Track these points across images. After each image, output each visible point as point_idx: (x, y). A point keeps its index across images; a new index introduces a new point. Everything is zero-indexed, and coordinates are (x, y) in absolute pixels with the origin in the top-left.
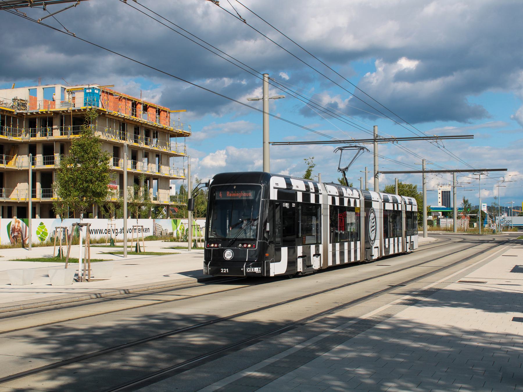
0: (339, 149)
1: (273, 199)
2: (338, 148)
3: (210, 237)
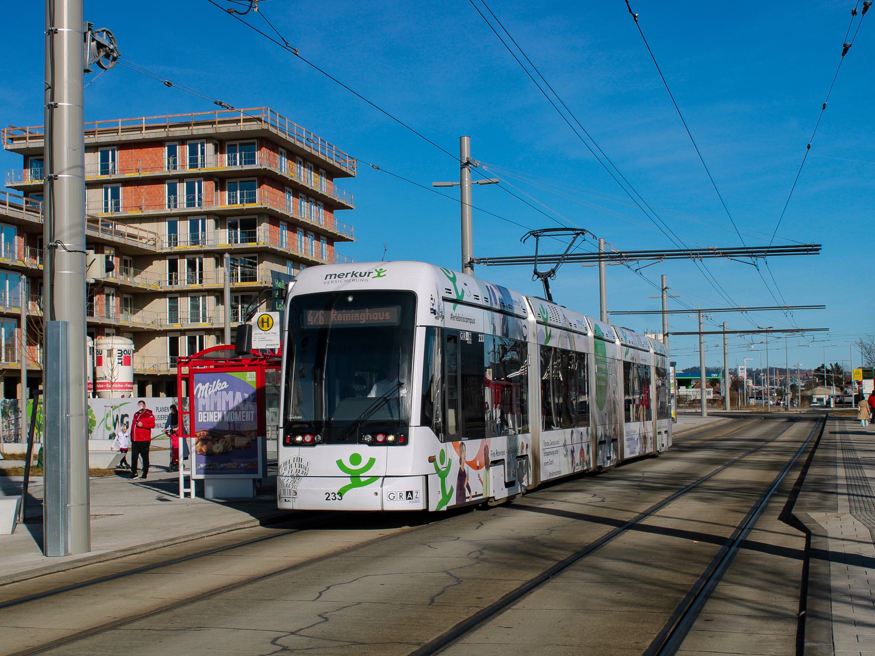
0: (531, 234)
1: (195, 378)
2: (530, 232)
3: (291, 418)
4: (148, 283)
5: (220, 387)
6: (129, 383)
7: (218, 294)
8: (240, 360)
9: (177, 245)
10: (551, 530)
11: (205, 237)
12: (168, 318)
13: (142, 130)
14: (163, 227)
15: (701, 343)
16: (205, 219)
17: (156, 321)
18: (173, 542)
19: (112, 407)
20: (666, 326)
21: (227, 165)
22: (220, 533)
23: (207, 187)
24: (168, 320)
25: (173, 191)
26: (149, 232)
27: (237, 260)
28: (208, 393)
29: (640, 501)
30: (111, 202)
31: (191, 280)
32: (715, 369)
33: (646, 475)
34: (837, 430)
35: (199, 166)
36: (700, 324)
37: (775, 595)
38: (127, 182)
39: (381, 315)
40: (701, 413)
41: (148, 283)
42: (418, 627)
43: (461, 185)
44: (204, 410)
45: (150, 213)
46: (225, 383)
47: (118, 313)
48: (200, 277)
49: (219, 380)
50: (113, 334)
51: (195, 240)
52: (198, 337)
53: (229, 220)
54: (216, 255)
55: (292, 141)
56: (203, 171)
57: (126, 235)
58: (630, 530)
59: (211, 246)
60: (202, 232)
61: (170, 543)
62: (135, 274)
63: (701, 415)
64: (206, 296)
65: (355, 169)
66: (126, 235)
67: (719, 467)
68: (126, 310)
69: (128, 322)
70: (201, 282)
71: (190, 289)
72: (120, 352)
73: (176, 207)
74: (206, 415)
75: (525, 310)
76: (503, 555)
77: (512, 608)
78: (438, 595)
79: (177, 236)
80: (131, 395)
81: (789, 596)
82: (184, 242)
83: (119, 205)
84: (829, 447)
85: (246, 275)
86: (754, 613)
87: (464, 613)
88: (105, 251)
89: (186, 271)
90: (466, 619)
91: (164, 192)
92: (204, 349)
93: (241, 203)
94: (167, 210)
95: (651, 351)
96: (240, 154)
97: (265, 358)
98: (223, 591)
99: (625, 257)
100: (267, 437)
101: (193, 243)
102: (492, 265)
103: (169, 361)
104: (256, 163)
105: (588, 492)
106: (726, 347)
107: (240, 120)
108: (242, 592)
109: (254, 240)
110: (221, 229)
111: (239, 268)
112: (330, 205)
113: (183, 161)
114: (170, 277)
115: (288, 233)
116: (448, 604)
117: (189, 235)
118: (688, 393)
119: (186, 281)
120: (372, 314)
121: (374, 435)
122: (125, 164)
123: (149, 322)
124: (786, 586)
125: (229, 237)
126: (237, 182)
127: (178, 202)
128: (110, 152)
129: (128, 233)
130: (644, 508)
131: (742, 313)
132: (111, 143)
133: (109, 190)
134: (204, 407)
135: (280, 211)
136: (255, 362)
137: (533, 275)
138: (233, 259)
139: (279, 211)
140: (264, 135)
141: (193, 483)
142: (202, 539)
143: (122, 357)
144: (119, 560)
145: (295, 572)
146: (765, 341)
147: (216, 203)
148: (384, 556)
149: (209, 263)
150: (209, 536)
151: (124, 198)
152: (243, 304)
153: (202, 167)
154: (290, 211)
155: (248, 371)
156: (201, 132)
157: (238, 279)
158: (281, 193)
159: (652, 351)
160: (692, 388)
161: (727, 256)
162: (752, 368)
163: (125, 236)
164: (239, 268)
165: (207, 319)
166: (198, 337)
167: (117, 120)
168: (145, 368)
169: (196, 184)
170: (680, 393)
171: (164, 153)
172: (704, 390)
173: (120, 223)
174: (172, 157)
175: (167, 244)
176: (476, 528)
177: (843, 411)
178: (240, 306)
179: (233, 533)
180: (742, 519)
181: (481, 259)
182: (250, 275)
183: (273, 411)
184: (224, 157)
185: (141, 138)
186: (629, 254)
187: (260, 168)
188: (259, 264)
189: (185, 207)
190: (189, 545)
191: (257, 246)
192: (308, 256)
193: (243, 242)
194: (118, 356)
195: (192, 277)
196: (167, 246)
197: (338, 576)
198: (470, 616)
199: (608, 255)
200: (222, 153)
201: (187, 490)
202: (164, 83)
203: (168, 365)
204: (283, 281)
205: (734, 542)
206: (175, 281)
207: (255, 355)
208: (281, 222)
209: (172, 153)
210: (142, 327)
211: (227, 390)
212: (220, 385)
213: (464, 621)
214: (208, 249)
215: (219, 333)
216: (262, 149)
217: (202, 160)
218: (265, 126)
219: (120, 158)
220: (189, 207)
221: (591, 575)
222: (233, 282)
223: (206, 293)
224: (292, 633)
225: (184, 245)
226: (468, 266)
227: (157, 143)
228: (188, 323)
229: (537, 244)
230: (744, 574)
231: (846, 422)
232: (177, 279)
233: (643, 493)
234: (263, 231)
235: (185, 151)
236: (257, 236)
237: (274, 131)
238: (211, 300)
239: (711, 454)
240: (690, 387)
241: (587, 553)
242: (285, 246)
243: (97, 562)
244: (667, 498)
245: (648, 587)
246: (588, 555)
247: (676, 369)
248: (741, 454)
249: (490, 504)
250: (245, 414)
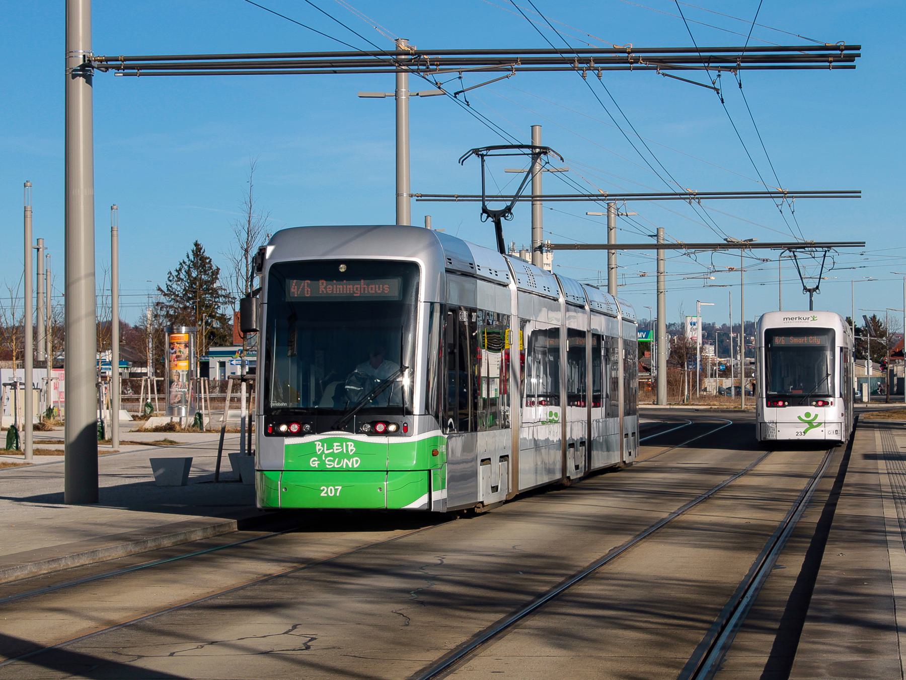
3: (272, 405)
15: (610, 269)
20: (538, 231)
32: (645, 323)
34: (879, 450)
36: (610, 229)
39: (379, 287)
67: (620, 540)
75: (472, 264)
84: (864, 492)
95: (618, 317)
102: (135, 75)
106: (662, 278)
120: (368, 285)
121: (374, 424)
131: (690, 203)
137: (482, 214)
146: (737, 266)
159: (619, 317)
162: (714, 324)
177: (887, 410)
181: (107, 60)
199: (389, 57)
226: (80, 75)
229: (483, 166)
231: (894, 432)
233: (421, 618)
239: (610, 504)
248: (675, 507)
249: (477, 511)
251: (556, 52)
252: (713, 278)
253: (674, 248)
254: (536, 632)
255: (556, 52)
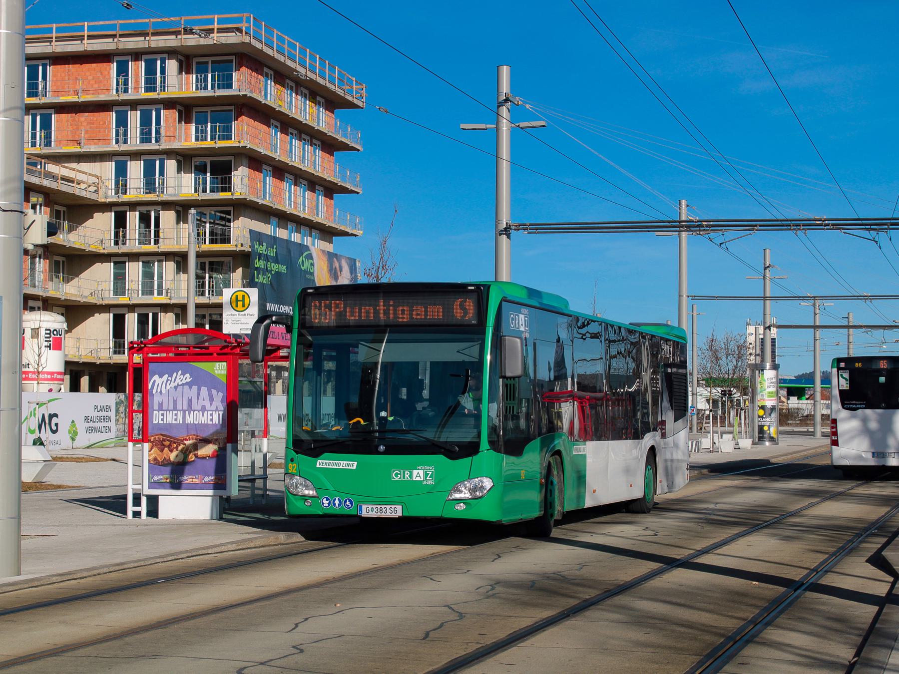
4: (86, 242)
5: (181, 381)
6: (59, 373)
7: (180, 259)
8: (207, 348)
9: (126, 193)
10: (582, 566)
11: (163, 183)
12: (112, 288)
13: (84, 39)
14: (108, 169)
16: (164, 159)
17: (97, 292)
18: (121, 567)
19: (37, 404)
21: (194, 89)
22: (177, 559)
23: (169, 116)
24: (112, 292)
25: (122, 122)
26: (90, 175)
27: (206, 214)
28: (166, 388)
29: (699, 536)
30: (41, 133)
31: (144, 240)
33: (719, 506)
35: (158, 89)
37: (830, 642)
38: (62, 108)
40: (813, 432)
41: (86, 242)
42: (406, 661)
43: (498, 129)
44: (161, 408)
45: (92, 150)
46: (188, 375)
47: (46, 280)
48: (155, 236)
49: (180, 372)
50: (39, 309)
51: (150, 186)
52: (151, 315)
53: (197, 161)
54: (178, 208)
55: (281, 58)
56: (163, 95)
57: (59, 178)
58: (680, 569)
59: (170, 195)
60: (159, 176)
61: (117, 568)
62: (71, 230)
63: (814, 436)
64: (162, 261)
65: (364, 98)
66: (59, 178)
68: (58, 277)
69: (59, 293)
70: (156, 242)
71: (142, 251)
72: (49, 332)
73: (125, 142)
74: (163, 415)
76: (519, 591)
77: (518, 645)
78: (434, 630)
79: (126, 181)
80: (60, 390)
81: (845, 643)
82: (136, 189)
83: (51, 137)
85: (216, 235)
86: (797, 659)
87: (462, 649)
88: (31, 198)
89: (137, 228)
90: (463, 654)
91: (110, 123)
92: (159, 334)
93: (212, 139)
94: (114, 147)
96: (212, 75)
97: (238, 346)
98: (182, 620)
99: (707, 227)
100: (239, 449)
101: (148, 191)
102: (534, 233)
103: (112, 345)
104: (234, 88)
105: (640, 525)
106: (851, 346)
107: (213, 29)
108: (204, 622)
109: (228, 189)
110: (184, 173)
111: (208, 225)
112: (330, 145)
113: (137, 82)
114: (117, 235)
115: (273, 180)
116: (444, 640)
117: (142, 180)
118: (800, 406)
119: (137, 241)
122: (59, 84)
123: (87, 293)
124: (849, 633)
125: (195, 184)
126: (207, 112)
127: (129, 136)
128: (40, 68)
129: (61, 175)
130: (700, 545)
132: (42, 56)
133: (38, 118)
134: (161, 405)
135: (263, 152)
136: (226, 351)
138: (201, 212)
139: (262, 151)
140: (241, 50)
141: (144, 500)
142: (156, 565)
143: (51, 339)
144: (56, 585)
145: (268, 602)
147: (179, 138)
148: (374, 588)
149: (168, 218)
150: (164, 562)
151: (57, 129)
152: (211, 273)
153: (161, 90)
154: (277, 152)
155: (216, 362)
156: (161, 44)
157: (205, 239)
158: (265, 127)
160: (807, 399)
161: (839, 229)
163: (58, 179)
164: (208, 225)
165: (164, 291)
166: (151, 315)
167: (50, 26)
168: (80, 353)
169: (154, 113)
170: (790, 406)
171: (111, 71)
172: (818, 403)
173: (52, 162)
174: (123, 76)
175: (113, 191)
176: (492, 560)
178: (207, 276)
179: (193, 560)
180: (822, 560)
182: (221, 235)
183: (247, 412)
184: (191, 79)
185: (82, 49)
186: (711, 223)
187: (238, 93)
188: (233, 222)
189: (138, 142)
190: (140, 571)
191: (231, 197)
192: (299, 211)
193: (214, 192)
194: (46, 338)
195: (145, 236)
196: (113, 194)
197: (318, 607)
198: (468, 652)
200: (188, 72)
201: (137, 509)
202: (123, 5)
203: (111, 350)
204: (265, 244)
205: (803, 584)
206: (123, 241)
207: (226, 341)
208: (264, 166)
209: (123, 70)
210: (78, 299)
211: (190, 384)
212: (182, 378)
213: (460, 657)
214: (167, 199)
215: (180, 311)
216: (241, 69)
217: (161, 81)
218: (246, 39)
219: (54, 76)
220: (143, 142)
221: (619, 616)
222: (199, 243)
223: (163, 258)
224: (261, 664)
225: (136, 193)
226: (503, 234)
227: (103, 57)
228: (138, 296)
230: (801, 619)
232: (125, 237)
233: (708, 528)
234: (240, 177)
235: (140, 69)
236: (233, 184)
237: (258, 45)
238: (170, 266)
240: (804, 398)
241: (618, 593)
242: (269, 197)
243: (29, 588)
244: (737, 534)
245: (682, 629)
246: (620, 595)
247: (779, 374)
250: (211, 415)
251: (777, 220)
252: (884, 347)
253: (855, 328)
254: (705, 521)
255: (777, 220)
